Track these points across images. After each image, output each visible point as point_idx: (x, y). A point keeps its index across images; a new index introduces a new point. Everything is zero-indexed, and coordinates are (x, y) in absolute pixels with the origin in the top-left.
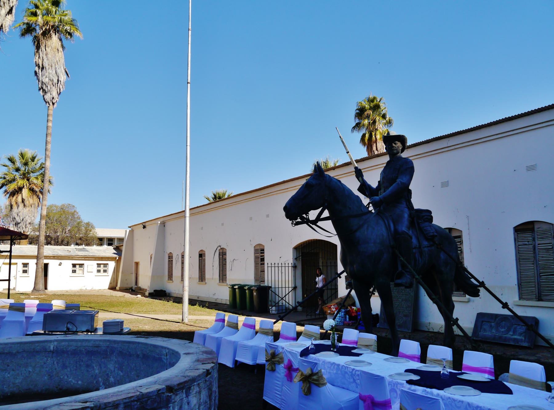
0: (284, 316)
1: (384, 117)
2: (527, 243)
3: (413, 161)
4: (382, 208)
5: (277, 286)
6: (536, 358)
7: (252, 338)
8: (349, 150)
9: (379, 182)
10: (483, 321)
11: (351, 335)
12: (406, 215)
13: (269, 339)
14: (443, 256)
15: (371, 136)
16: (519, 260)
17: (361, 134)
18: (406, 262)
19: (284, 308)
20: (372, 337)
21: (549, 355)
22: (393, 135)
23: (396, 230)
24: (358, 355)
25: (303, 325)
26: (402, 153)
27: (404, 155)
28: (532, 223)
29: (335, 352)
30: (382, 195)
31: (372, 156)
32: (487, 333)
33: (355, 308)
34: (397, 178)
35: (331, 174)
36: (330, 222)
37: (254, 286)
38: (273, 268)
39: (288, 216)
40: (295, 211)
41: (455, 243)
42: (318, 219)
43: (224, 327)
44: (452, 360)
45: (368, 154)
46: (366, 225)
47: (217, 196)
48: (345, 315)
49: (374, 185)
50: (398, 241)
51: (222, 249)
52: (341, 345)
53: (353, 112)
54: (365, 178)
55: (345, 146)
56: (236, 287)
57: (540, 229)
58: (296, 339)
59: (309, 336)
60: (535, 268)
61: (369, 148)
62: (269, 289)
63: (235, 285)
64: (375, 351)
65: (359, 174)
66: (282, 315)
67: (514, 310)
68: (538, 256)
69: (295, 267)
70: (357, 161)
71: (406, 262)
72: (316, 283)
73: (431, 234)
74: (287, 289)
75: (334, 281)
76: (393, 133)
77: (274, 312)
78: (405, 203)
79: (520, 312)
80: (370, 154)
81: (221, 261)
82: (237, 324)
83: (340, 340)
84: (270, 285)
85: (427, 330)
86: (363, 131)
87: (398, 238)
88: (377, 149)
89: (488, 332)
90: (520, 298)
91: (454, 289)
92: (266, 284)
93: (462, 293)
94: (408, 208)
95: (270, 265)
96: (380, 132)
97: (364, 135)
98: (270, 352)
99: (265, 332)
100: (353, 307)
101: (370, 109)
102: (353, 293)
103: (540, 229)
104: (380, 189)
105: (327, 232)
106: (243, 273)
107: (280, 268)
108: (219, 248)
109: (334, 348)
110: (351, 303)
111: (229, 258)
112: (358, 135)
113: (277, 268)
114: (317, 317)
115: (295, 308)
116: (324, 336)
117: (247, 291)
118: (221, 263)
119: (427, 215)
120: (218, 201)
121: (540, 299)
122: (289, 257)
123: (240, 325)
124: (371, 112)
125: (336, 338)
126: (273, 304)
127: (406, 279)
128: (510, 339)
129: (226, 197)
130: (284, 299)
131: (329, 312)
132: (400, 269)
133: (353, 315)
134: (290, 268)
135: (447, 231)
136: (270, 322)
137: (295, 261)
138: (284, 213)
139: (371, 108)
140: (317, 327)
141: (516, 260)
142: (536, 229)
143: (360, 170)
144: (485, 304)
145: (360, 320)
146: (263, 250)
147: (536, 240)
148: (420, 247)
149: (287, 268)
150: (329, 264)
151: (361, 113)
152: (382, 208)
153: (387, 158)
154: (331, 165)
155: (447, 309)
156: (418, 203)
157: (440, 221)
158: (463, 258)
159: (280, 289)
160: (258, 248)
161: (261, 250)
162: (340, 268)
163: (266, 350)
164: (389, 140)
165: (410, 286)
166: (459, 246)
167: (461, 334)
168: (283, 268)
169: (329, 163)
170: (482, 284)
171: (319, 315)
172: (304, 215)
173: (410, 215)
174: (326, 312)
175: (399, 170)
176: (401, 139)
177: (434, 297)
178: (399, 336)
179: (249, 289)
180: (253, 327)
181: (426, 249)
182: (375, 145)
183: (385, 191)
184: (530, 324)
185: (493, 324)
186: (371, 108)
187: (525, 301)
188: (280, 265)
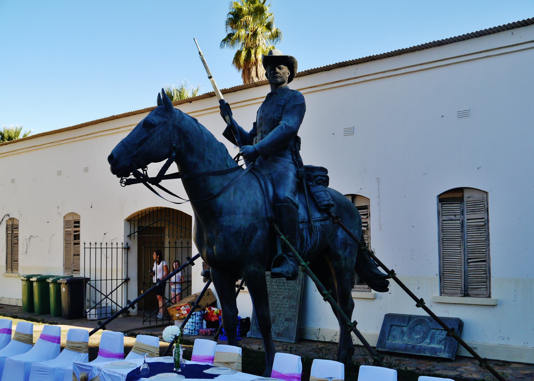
0: (106, 323)
1: (269, 27)
2: (453, 217)
3: (305, 96)
4: (257, 163)
5: (98, 278)
6: (457, 373)
7: (55, 356)
8: (212, 74)
9: (255, 124)
10: (392, 325)
11: (204, 348)
12: (291, 175)
13: (82, 358)
14: (341, 234)
15: (249, 54)
16: (443, 241)
17: (234, 52)
18: (288, 242)
19: (109, 311)
20: (236, 351)
21: (474, 369)
22: (278, 55)
23: (275, 194)
24: (212, 376)
25: (134, 336)
26: (289, 82)
27: (293, 86)
28: (461, 190)
29: (179, 373)
30: (258, 143)
31: (249, 85)
32: (397, 342)
33: (215, 309)
34: (280, 119)
35: (185, 109)
36: (179, 181)
37: (63, 278)
38: (93, 250)
39: (114, 171)
40: (127, 163)
41: (359, 216)
42: (162, 176)
43: (10, 340)
44: (343, 379)
45: (245, 82)
46: (233, 188)
47: (6, 135)
48: (201, 320)
49: (248, 128)
50: (278, 213)
51: (12, 219)
52: (188, 362)
53: (224, 15)
54: (234, 117)
55: (206, 67)
56: (34, 279)
57: (471, 199)
58: (123, 356)
59: (142, 350)
60: (462, 252)
61: (246, 73)
62: (86, 282)
63: (32, 276)
64: (239, 370)
65: (225, 110)
66: (103, 321)
67: (432, 310)
68: (466, 235)
69: (127, 249)
70: (224, 92)
71: (288, 242)
72: (153, 273)
73: (326, 203)
74: (114, 282)
75: (186, 268)
76: (278, 52)
77: (93, 317)
78: (290, 156)
79: (440, 312)
80: (247, 82)
81: (10, 238)
82: (31, 336)
83: (188, 355)
84: (87, 276)
85: (316, 339)
86: (238, 46)
87: (279, 209)
88: (257, 75)
89: (399, 341)
90: (441, 293)
91: (356, 281)
92: (81, 275)
93: (367, 286)
94: (295, 164)
95: (88, 245)
96: (263, 50)
97: (239, 53)
98: (80, 376)
99: (75, 348)
100: (213, 309)
101: (249, 15)
102: (212, 286)
103: (471, 199)
104: (256, 135)
105: (175, 197)
106: (45, 258)
107: (104, 250)
108: (7, 218)
109: (177, 368)
110: (210, 302)
111: (23, 234)
112: (230, 52)
113: (99, 250)
114: (160, 323)
115: (125, 311)
116: (165, 351)
117: (51, 286)
118: (10, 243)
119: (319, 176)
120: (6, 144)
121: (466, 294)
122: (118, 234)
123: (36, 337)
124: (250, 18)
125: (181, 353)
126: (93, 305)
127: (288, 267)
128: (425, 349)
129: (21, 137)
130: (110, 297)
131: (177, 315)
132: (280, 252)
133: (213, 319)
134: (120, 250)
135: (350, 199)
136: (84, 331)
137: (128, 240)
138: (109, 166)
139: (250, 13)
140: (157, 338)
141: (439, 241)
142: (465, 199)
143: (227, 105)
144: (395, 301)
145: (222, 327)
146: (78, 222)
147: (465, 213)
148: (309, 221)
149: (114, 250)
150: (180, 245)
151: (236, 18)
152: (257, 163)
153: (267, 90)
154: (188, 95)
155: (343, 309)
156: (309, 156)
157: (339, 184)
158: (369, 238)
159: (104, 282)
160: (70, 218)
161: (75, 223)
162: (195, 251)
163: (74, 374)
164: (272, 62)
165: (293, 276)
166: (363, 221)
167: (361, 344)
168: (109, 250)
169: (186, 91)
170: (392, 274)
171: (163, 320)
172: (140, 170)
173: (297, 175)
174: (173, 316)
175: (284, 107)
176: (289, 62)
177: (325, 292)
178: (276, 348)
179: (55, 282)
180: (57, 340)
181: (318, 224)
182: (254, 68)
183: (262, 138)
184: (451, 328)
185: (405, 329)
186: (250, 13)
187: (447, 297)
188: (104, 246)
